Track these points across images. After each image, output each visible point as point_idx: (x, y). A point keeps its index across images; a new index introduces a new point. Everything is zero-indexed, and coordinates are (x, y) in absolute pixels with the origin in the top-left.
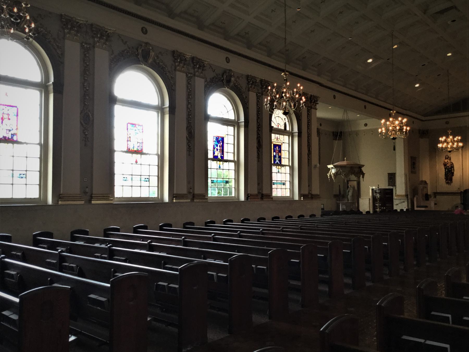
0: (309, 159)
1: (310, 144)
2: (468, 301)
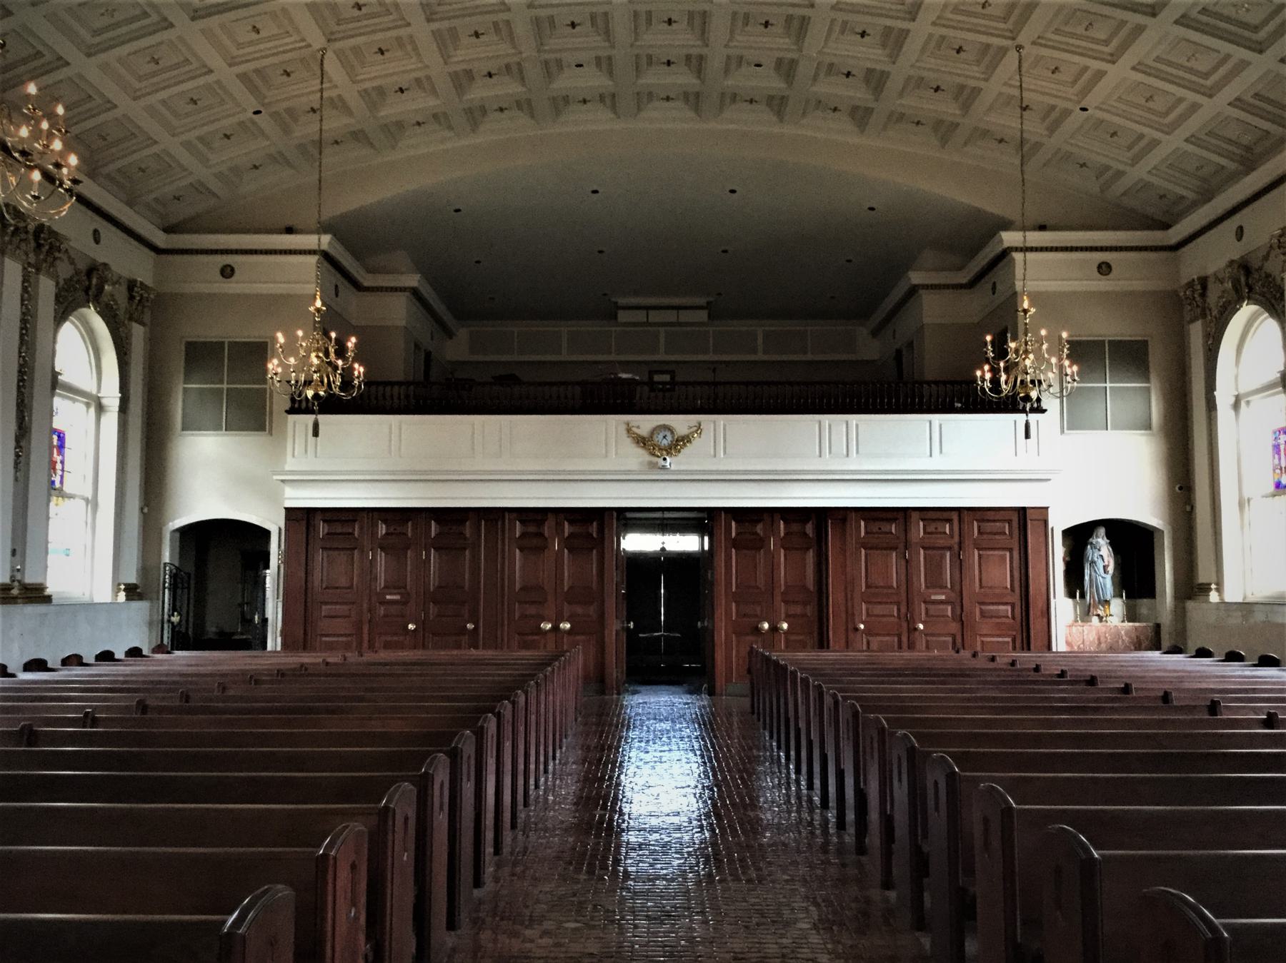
0: (20, 456)
1: (26, 401)
2: (328, 961)
